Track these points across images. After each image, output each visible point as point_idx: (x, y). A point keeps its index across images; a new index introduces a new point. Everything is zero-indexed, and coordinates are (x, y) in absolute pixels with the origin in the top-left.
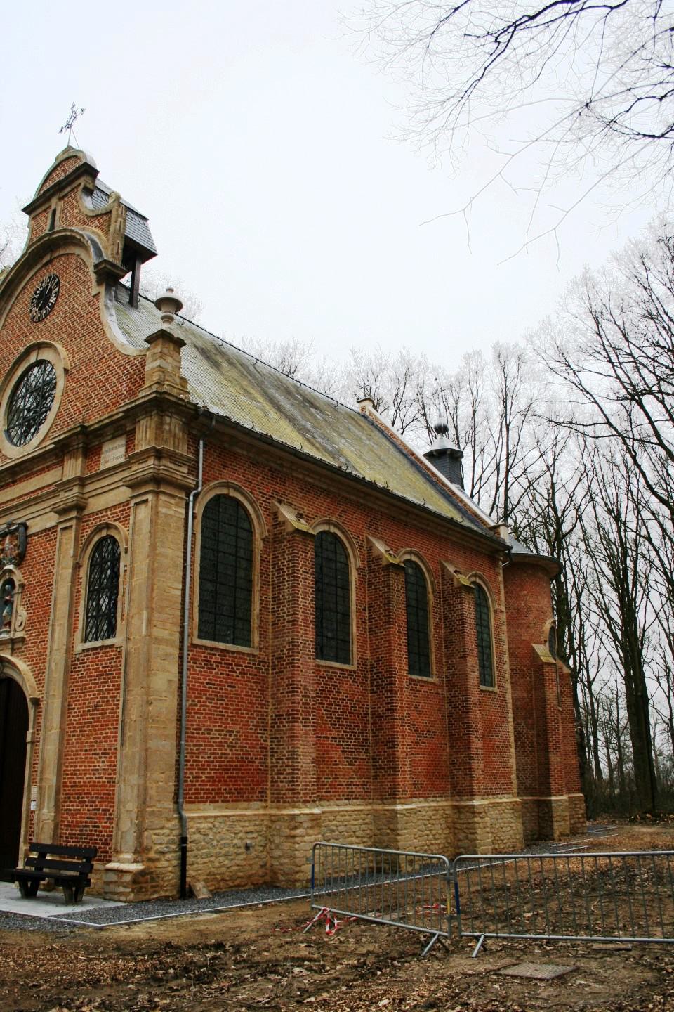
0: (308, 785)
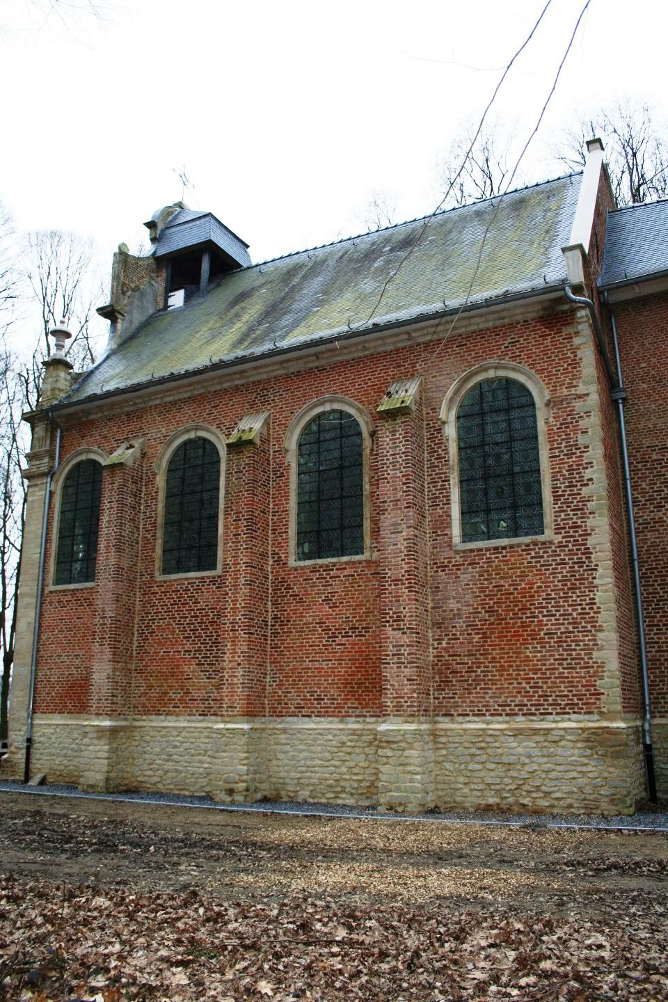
0: (101, 700)
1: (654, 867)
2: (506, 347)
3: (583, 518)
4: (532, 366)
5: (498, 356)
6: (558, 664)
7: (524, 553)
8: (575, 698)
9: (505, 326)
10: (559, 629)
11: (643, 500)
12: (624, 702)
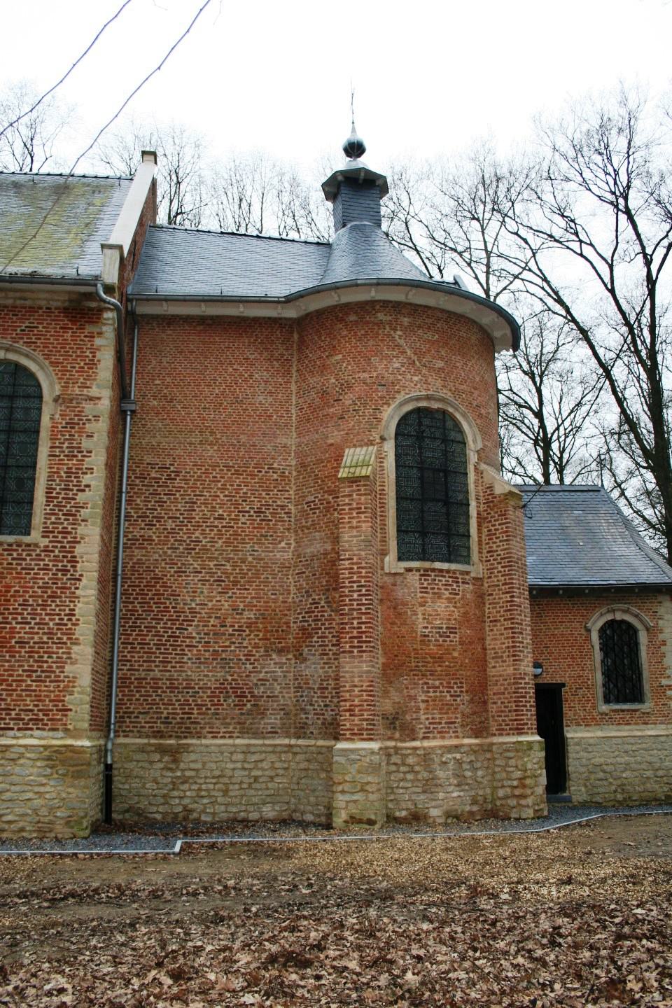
1: (113, 893)
2: (22, 330)
3: (75, 524)
4: (47, 356)
5: (12, 338)
6: (27, 676)
7: (6, 553)
8: (41, 714)
9: (25, 308)
10: (33, 638)
11: (135, 515)
12: (91, 720)
